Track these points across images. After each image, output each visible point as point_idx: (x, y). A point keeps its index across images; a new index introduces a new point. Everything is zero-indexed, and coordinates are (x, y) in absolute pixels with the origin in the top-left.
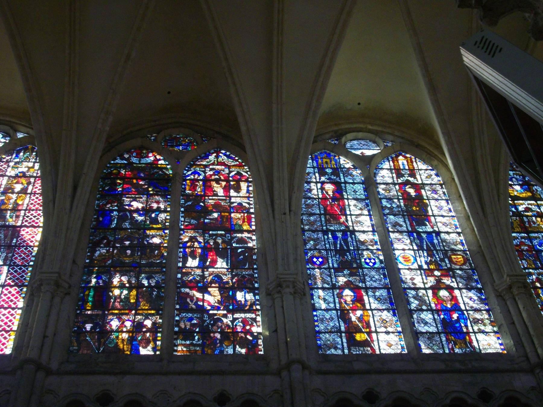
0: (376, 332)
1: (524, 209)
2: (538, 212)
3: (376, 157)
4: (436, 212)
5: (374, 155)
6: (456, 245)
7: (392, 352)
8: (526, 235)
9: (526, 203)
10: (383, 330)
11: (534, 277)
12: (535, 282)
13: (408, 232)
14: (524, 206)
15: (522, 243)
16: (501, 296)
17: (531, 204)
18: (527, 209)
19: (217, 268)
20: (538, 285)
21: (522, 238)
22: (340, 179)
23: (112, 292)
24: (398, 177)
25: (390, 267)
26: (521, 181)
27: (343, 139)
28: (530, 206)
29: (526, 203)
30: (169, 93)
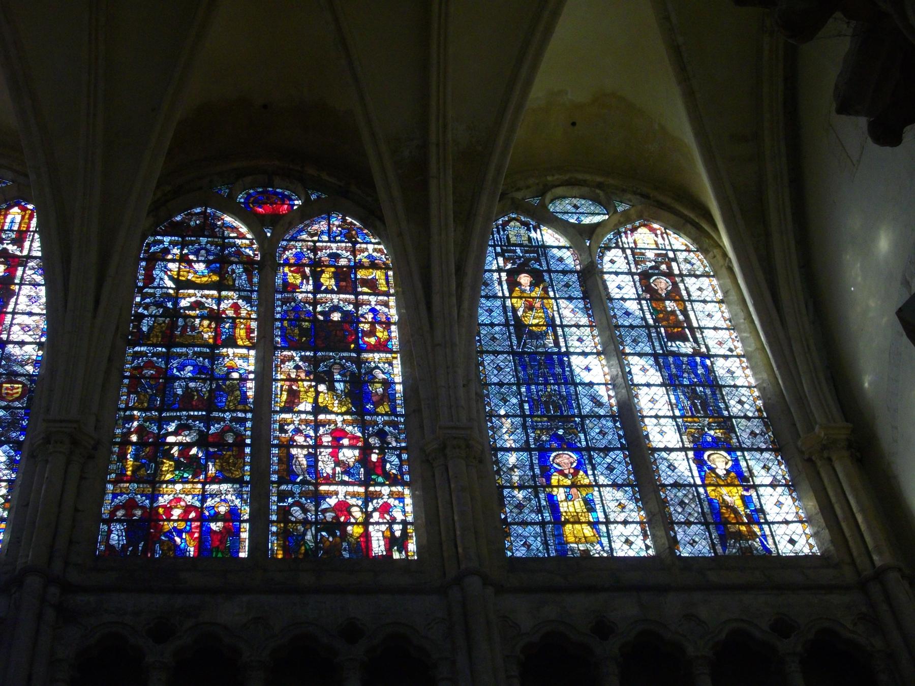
0: (607, 522)
1: (189, 305)
2: (212, 310)
3: (599, 230)
4: (705, 322)
5: (598, 224)
6: (22, 366)
7: (632, 554)
8: (164, 350)
9: (195, 295)
10: (621, 518)
11: (136, 424)
12: (132, 433)
13: (655, 356)
14: (193, 299)
15: (150, 365)
16: (428, 461)
17: (207, 297)
18: (193, 306)
19: (300, 412)
20: (134, 438)
21: (154, 355)
22: (541, 265)
23: (378, 454)
24: (637, 263)
25: (628, 416)
26: (214, 254)
27: (549, 196)
28: (204, 300)
29: (199, 295)
30: (574, 124)
